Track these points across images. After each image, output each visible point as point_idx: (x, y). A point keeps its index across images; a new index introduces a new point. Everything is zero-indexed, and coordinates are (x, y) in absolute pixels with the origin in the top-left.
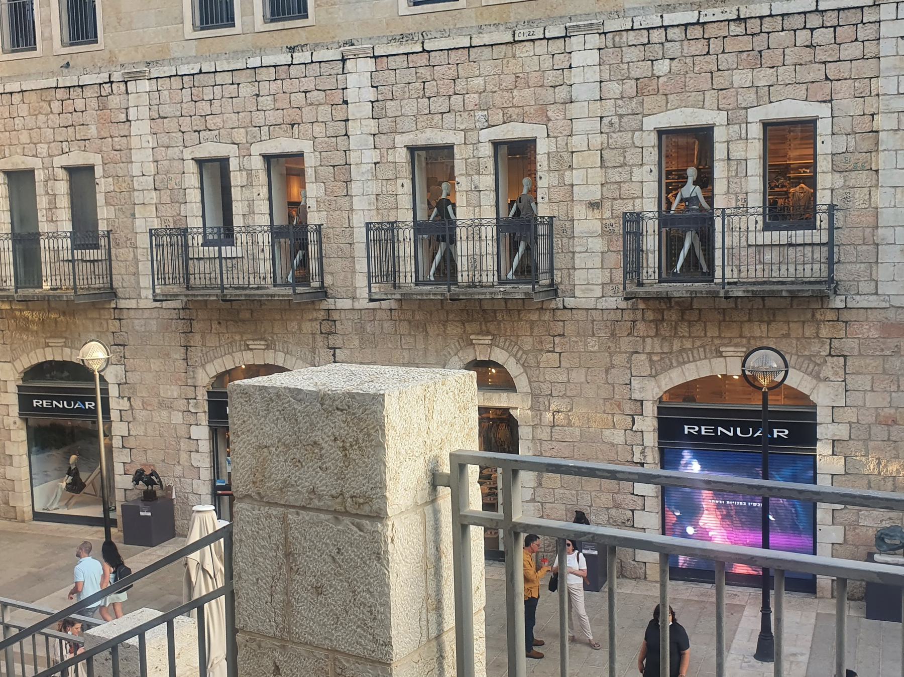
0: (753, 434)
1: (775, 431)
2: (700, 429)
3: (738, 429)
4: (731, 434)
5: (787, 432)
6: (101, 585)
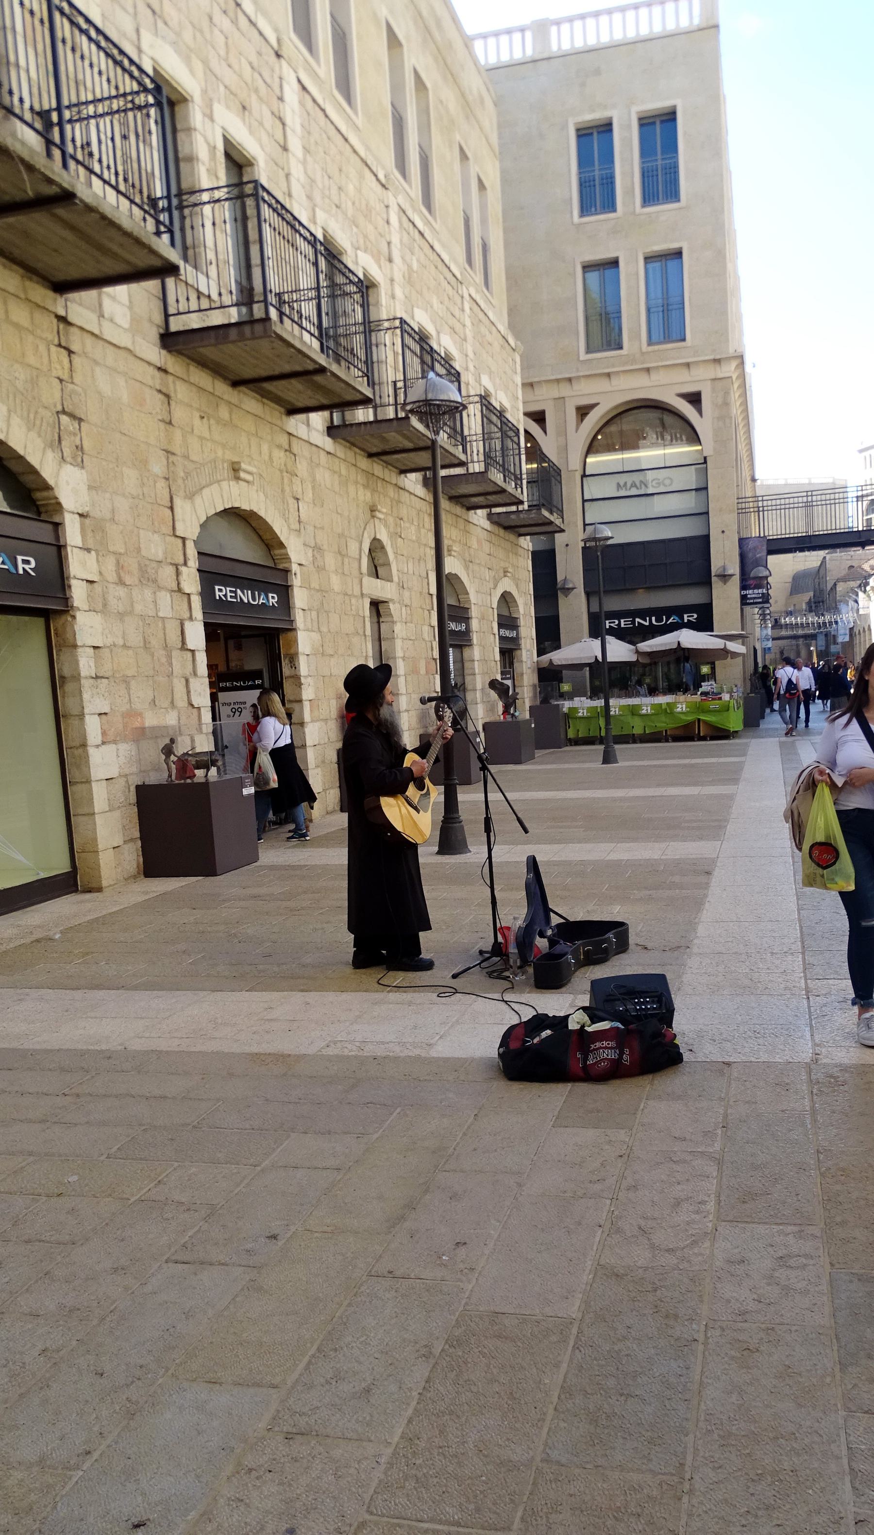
0: (667, 620)
1: (685, 616)
2: (620, 622)
3: (653, 618)
4: (647, 624)
5: (695, 616)
6: (441, 447)
